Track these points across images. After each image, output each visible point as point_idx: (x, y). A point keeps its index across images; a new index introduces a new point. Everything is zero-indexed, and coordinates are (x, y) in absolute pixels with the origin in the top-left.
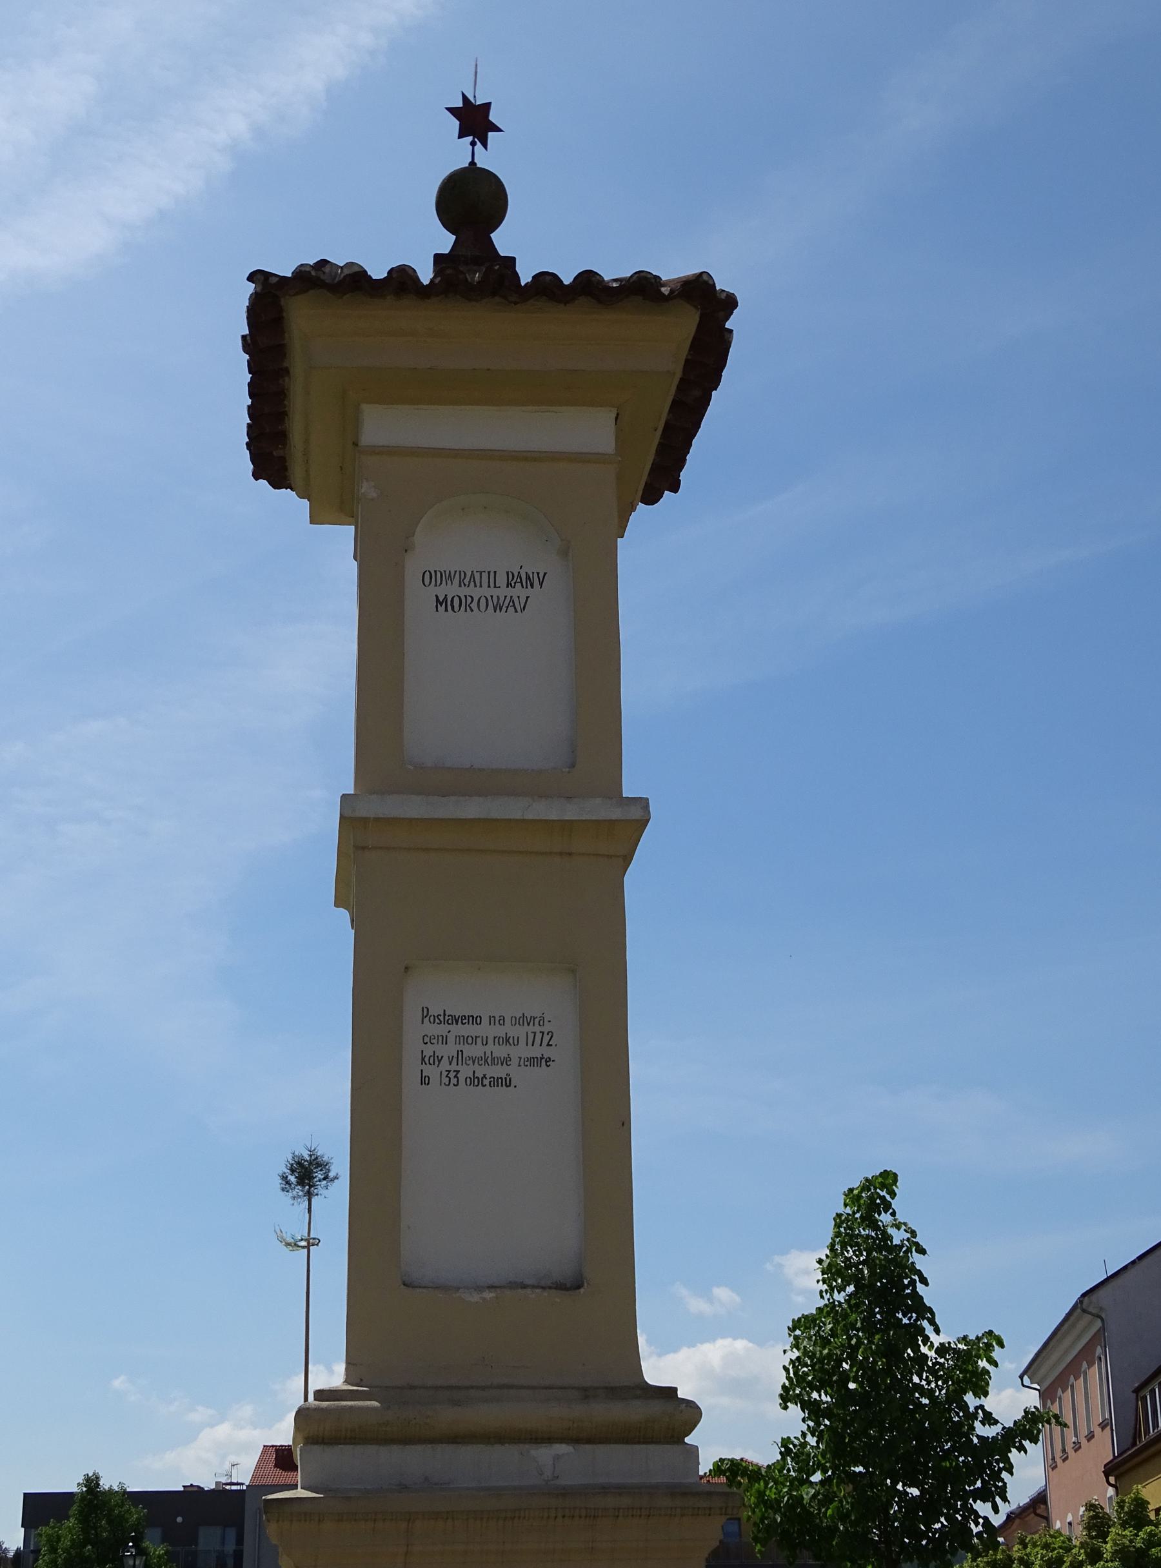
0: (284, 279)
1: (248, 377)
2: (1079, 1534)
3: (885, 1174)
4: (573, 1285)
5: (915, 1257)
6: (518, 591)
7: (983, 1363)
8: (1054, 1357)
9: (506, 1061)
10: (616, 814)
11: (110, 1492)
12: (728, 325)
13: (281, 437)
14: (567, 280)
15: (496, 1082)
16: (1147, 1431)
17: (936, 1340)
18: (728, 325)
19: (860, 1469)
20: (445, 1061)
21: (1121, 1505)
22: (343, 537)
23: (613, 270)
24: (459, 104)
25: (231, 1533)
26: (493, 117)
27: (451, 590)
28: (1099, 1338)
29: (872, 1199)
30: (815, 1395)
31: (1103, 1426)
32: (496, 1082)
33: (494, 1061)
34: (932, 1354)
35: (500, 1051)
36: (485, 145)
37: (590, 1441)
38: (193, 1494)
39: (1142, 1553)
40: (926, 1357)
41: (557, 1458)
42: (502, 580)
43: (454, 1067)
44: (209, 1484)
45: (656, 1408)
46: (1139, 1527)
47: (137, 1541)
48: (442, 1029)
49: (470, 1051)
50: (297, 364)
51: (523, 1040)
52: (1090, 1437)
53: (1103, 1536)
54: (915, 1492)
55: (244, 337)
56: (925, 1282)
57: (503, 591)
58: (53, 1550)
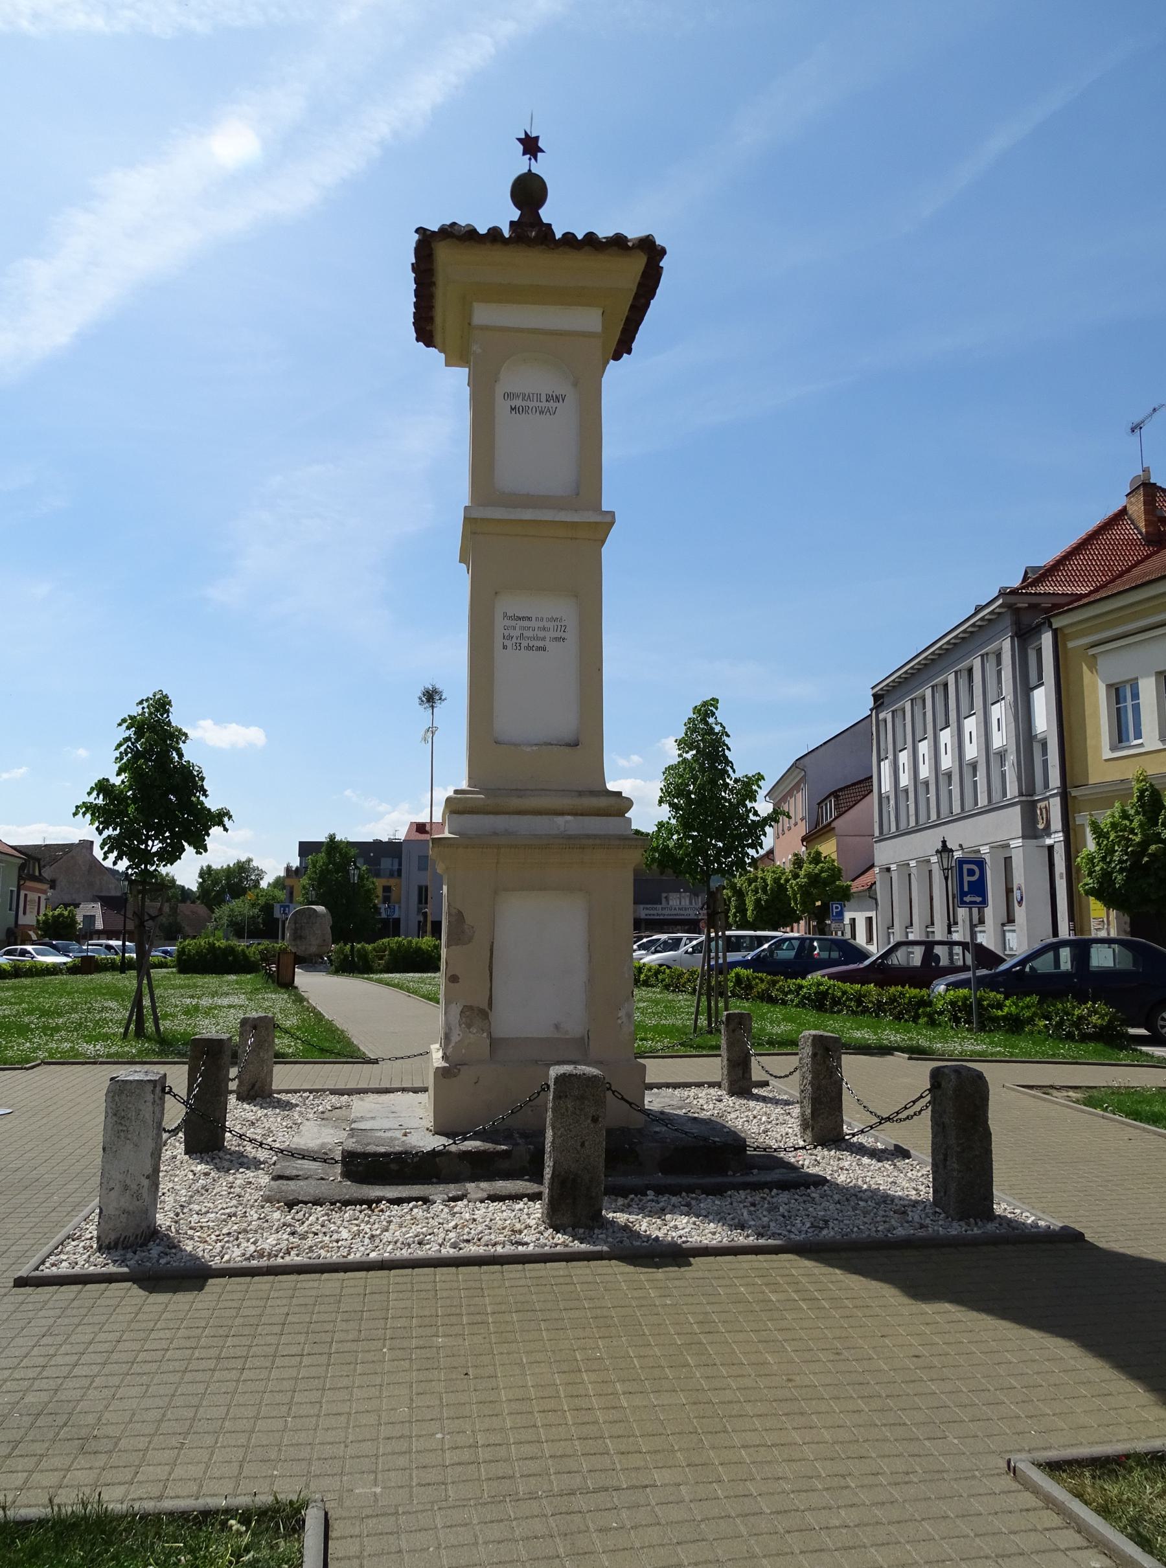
0: (434, 232)
1: (414, 286)
2: (789, 867)
3: (713, 699)
4: (575, 744)
5: (725, 738)
6: (552, 404)
7: (755, 787)
8: (781, 788)
9: (544, 639)
10: (598, 519)
11: (341, 842)
12: (661, 265)
13: (431, 320)
14: (580, 237)
15: (539, 649)
16: (822, 822)
17: (733, 776)
18: (661, 265)
19: (695, 834)
20: (515, 638)
21: (809, 854)
22: (461, 374)
23: (604, 232)
24: (523, 136)
25: (396, 861)
26: (521, 147)
27: (518, 403)
28: (803, 780)
29: (706, 711)
30: (676, 800)
31: (802, 820)
32: (539, 649)
33: (538, 638)
34: (731, 782)
35: (541, 634)
36: (536, 160)
37: (582, 815)
38: (377, 844)
39: (818, 875)
40: (728, 784)
41: (566, 822)
42: (544, 398)
43: (519, 641)
44: (385, 839)
45: (612, 800)
46: (817, 864)
47: (355, 863)
48: (513, 623)
49: (526, 633)
50: (440, 278)
51: (552, 629)
52: (796, 824)
53: (801, 868)
54: (720, 844)
55: (413, 264)
56: (729, 749)
57: (544, 404)
58: (314, 866)
